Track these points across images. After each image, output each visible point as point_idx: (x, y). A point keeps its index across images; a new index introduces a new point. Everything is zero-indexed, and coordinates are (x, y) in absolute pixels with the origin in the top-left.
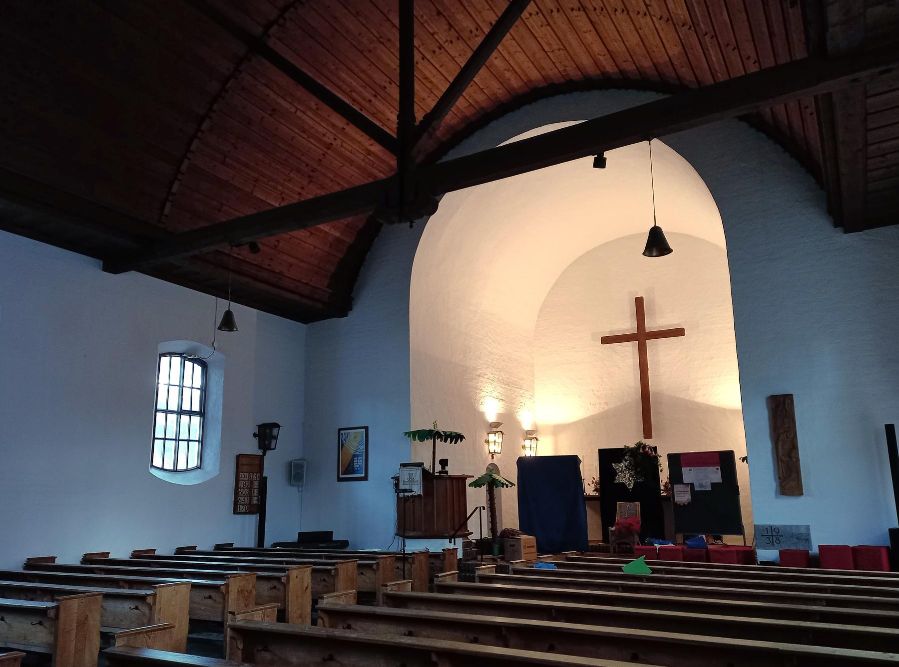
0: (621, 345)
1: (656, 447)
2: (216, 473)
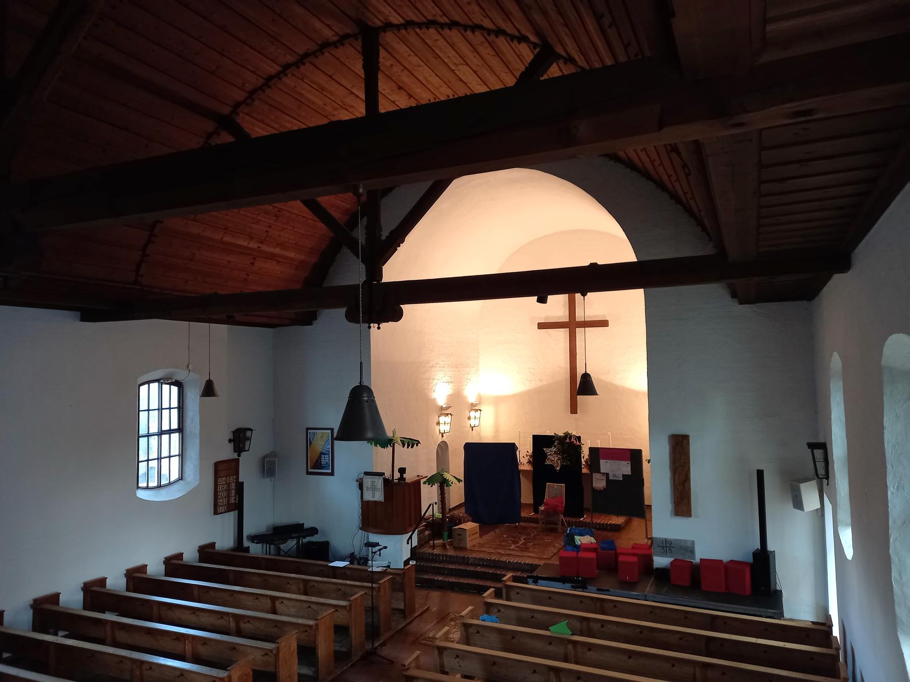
1: (580, 437)
2: (197, 483)
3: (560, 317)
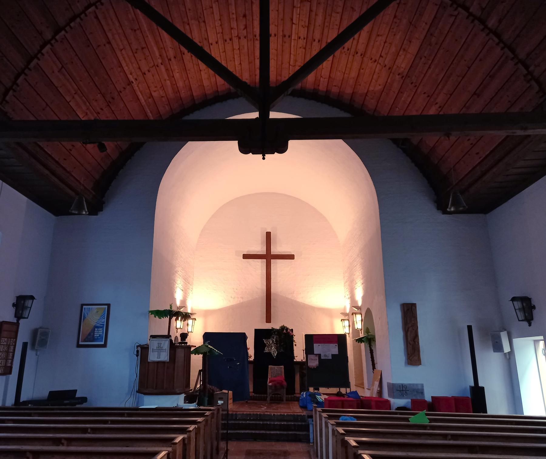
0: (254, 261)
3: (258, 252)
